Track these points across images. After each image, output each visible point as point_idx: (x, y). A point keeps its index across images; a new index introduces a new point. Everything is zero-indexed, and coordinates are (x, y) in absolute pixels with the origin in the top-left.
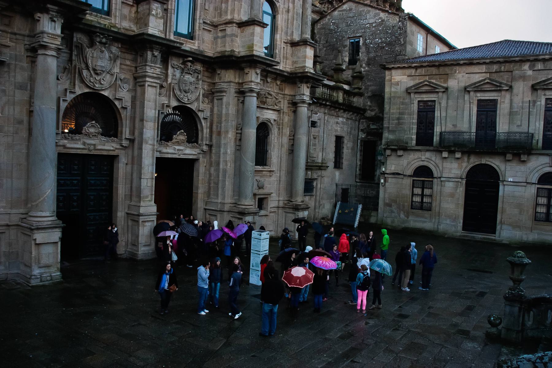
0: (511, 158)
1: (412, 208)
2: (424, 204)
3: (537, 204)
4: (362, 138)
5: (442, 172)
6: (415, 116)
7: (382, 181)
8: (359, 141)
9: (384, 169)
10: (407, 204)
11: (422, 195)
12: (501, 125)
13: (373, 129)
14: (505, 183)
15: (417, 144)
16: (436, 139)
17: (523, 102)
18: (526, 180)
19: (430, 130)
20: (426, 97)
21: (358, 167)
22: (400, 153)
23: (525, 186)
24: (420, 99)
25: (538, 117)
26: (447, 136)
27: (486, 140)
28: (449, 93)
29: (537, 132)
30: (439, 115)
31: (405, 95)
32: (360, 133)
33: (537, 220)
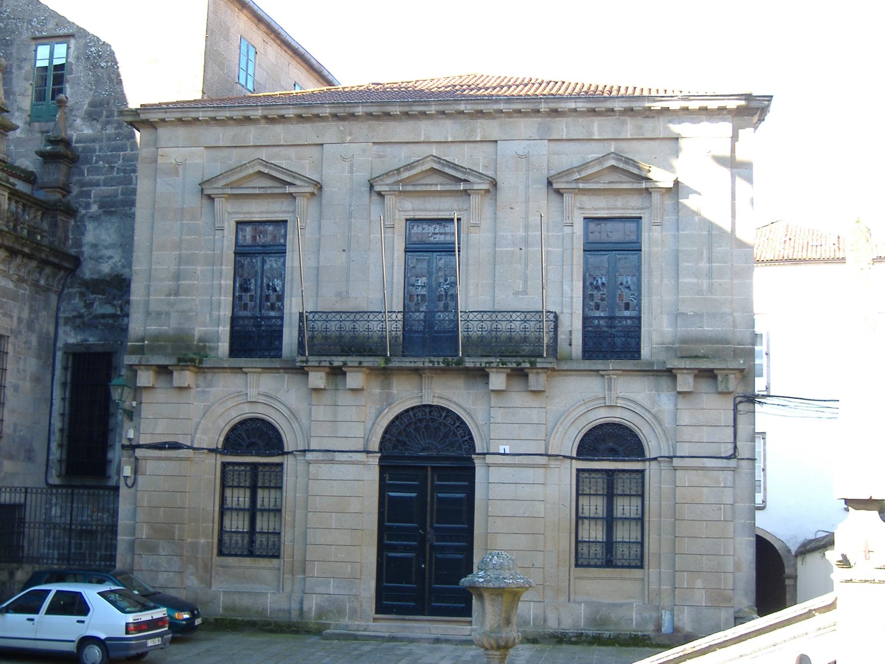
0: (502, 387)
1: (221, 553)
2: (259, 539)
3: (578, 518)
4: (66, 345)
5: (308, 437)
6: (228, 268)
7: (127, 471)
8: (59, 354)
9: (131, 434)
10: (208, 539)
11: (253, 512)
12: (471, 293)
13: (104, 316)
14: (489, 459)
15: (234, 352)
16: (290, 337)
17: (527, 227)
18: (547, 448)
19: (272, 308)
20: (258, 211)
21: (56, 437)
22: (185, 377)
23: (545, 466)
24: (241, 218)
25: (567, 268)
26: (319, 325)
27: (431, 337)
28: (324, 201)
29: (566, 310)
30: (296, 264)
31: (194, 201)
32: (61, 330)
33: (582, 566)
